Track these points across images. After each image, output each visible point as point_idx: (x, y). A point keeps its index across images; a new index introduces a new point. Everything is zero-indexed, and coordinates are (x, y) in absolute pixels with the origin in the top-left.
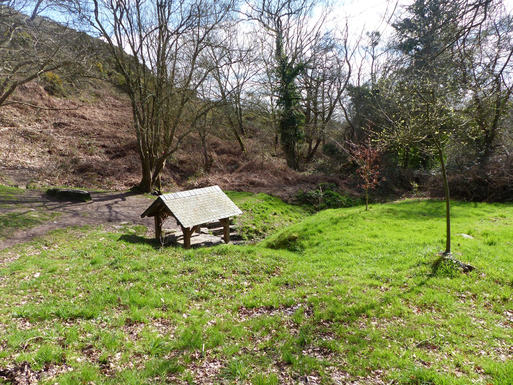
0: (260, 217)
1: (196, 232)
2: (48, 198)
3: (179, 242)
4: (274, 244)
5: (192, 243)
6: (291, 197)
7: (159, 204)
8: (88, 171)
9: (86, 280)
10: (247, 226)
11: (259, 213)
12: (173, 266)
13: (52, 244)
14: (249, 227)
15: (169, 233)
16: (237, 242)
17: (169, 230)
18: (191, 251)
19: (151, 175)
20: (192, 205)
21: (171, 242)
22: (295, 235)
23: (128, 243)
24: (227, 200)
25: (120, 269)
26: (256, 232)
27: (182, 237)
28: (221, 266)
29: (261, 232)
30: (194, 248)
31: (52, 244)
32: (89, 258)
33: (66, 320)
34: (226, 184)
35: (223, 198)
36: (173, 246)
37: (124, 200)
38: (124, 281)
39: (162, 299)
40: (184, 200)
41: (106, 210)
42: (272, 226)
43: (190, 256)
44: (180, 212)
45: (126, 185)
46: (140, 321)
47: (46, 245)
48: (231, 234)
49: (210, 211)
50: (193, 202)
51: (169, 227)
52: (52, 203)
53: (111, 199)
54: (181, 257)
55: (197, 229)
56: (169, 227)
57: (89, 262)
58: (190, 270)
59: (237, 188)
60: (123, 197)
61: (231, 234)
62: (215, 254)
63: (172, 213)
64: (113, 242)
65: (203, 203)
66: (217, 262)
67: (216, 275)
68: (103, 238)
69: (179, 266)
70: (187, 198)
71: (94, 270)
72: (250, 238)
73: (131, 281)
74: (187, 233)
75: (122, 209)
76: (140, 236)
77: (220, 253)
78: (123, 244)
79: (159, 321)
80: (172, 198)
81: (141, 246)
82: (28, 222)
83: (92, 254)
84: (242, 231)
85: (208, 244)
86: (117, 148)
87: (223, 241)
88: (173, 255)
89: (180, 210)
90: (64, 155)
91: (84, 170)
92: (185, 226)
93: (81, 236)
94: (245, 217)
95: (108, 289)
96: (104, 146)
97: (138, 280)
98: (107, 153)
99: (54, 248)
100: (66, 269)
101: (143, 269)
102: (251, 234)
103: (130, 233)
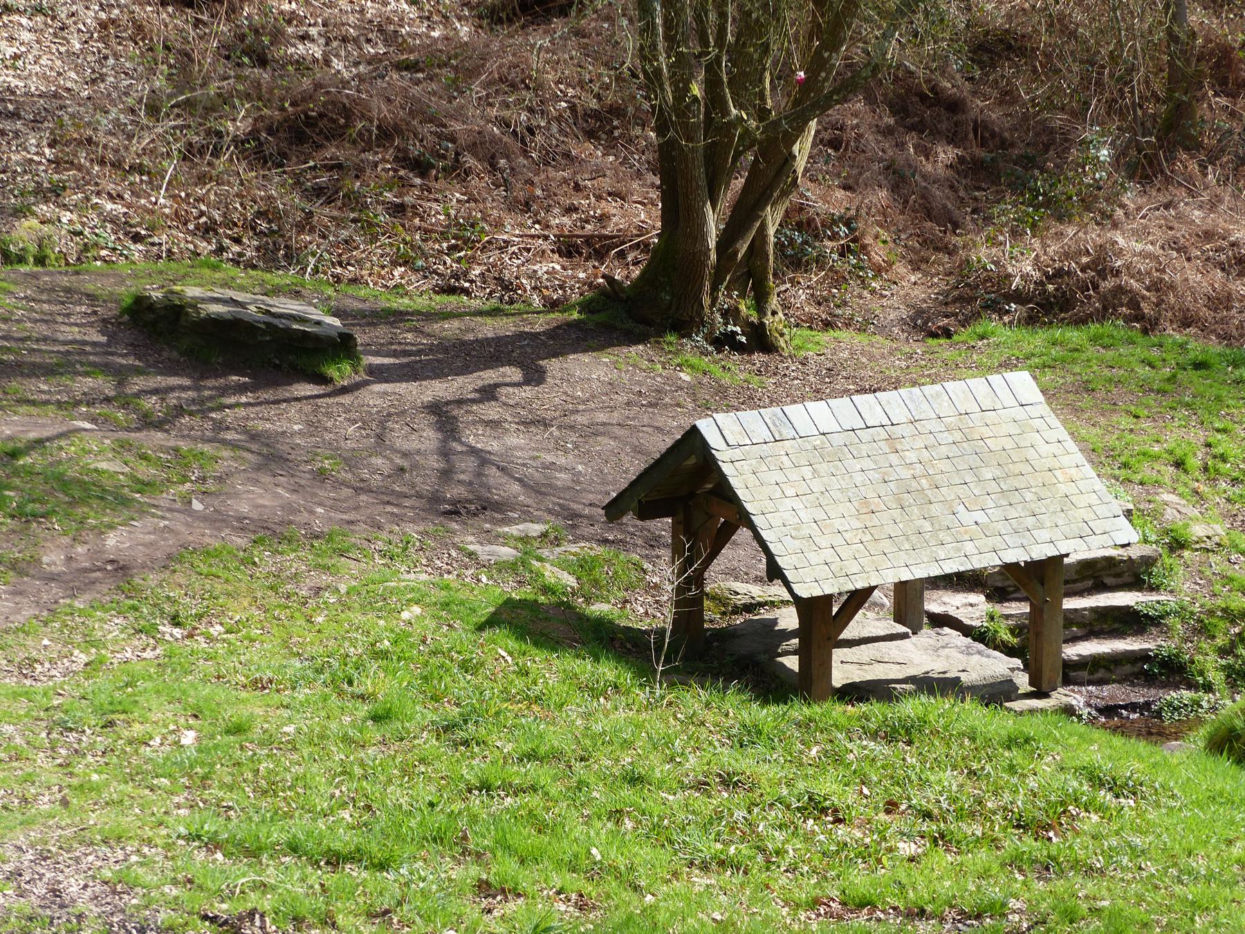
2: (135, 349)
5: (839, 677)
7: (692, 461)
8: (337, 134)
9: (358, 771)
13: (199, 617)
15: (750, 608)
18: (840, 711)
19: (713, 224)
20: (859, 478)
23: (528, 647)
24: (1065, 460)
25: (476, 749)
31: (199, 617)
32: (362, 697)
33: (317, 862)
35: (1044, 449)
37: (535, 376)
38: (485, 787)
39: (594, 851)
40: (825, 451)
41: (428, 438)
45: (568, 249)
46: (515, 889)
47: (175, 621)
49: (948, 520)
50: (867, 464)
51: (732, 578)
53: (465, 370)
57: (364, 709)
58: (728, 781)
60: (529, 355)
64: (460, 636)
65: (919, 469)
67: (816, 807)
68: (417, 610)
70: (838, 440)
71: (384, 743)
73: (518, 791)
74: (824, 620)
75: (514, 440)
76: (599, 609)
77: (889, 734)
78: (503, 648)
79: (569, 900)
81: (584, 667)
82: (81, 494)
83: (376, 681)
84: (1202, 630)
91: (304, 131)
93: (318, 591)
95: (432, 805)
99: (210, 639)
100: (286, 729)
101: (556, 756)
103: (546, 590)
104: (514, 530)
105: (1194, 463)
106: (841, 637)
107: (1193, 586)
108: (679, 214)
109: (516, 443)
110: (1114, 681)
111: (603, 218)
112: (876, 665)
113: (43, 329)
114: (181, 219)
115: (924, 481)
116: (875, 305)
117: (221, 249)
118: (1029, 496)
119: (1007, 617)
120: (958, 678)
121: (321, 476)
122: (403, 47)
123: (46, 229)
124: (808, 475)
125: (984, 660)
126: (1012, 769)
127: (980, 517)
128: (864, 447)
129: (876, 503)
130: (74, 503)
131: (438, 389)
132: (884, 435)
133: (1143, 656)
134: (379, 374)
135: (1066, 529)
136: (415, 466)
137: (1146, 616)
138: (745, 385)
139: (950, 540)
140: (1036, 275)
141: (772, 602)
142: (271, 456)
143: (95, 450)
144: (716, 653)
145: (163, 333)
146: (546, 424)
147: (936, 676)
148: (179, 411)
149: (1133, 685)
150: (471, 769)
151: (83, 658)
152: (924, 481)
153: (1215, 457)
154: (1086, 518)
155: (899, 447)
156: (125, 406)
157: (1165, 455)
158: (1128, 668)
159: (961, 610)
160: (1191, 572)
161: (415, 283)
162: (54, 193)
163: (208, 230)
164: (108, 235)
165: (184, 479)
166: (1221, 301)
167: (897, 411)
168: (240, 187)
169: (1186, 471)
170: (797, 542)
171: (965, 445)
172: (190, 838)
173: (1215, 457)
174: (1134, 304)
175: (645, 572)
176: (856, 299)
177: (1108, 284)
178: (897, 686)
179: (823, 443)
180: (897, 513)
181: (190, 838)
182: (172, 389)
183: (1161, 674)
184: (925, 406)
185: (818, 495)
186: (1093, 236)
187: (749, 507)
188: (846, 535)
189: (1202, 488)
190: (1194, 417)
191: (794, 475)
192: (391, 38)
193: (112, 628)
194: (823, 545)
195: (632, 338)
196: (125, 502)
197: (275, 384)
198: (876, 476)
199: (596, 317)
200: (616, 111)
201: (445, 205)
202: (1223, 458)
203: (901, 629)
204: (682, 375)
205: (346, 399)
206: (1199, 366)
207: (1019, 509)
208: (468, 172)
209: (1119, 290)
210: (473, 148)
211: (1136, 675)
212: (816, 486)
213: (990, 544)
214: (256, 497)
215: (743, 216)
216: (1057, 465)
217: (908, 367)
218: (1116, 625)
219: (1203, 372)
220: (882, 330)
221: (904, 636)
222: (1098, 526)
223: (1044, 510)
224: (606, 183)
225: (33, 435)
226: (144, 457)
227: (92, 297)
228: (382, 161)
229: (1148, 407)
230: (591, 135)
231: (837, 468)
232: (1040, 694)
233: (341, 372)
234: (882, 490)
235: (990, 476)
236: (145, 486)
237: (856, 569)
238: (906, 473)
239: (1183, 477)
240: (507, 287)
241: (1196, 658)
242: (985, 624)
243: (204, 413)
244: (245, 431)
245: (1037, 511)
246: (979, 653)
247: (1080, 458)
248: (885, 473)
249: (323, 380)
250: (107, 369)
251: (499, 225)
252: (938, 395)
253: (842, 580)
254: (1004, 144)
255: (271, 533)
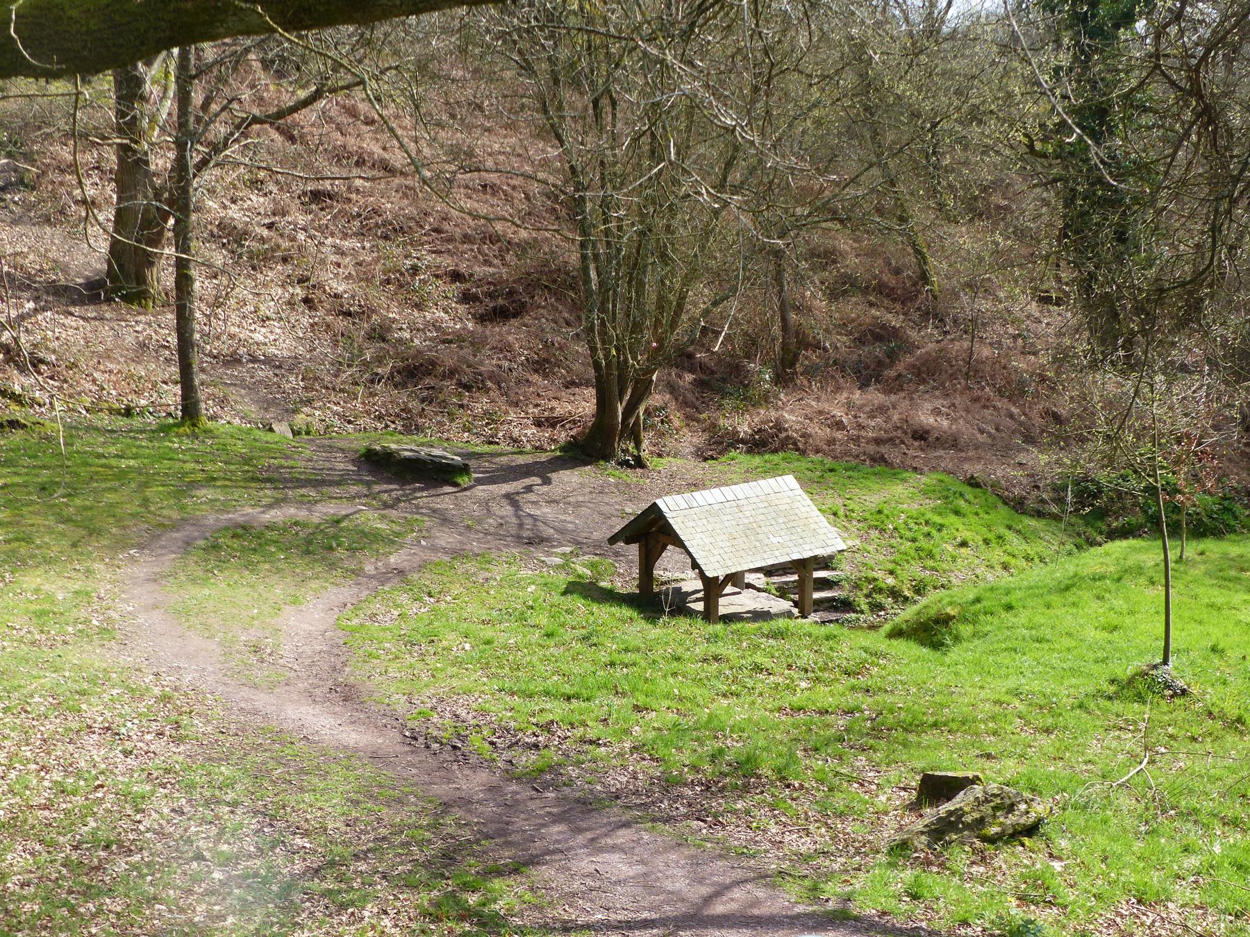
0: (913, 553)
2: (370, 473)
3: (692, 605)
4: (904, 627)
5: (722, 611)
6: (1037, 487)
10: (871, 574)
11: (914, 540)
14: (875, 580)
16: (833, 616)
17: (669, 574)
18: (719, 627)
20: (727, 524)
21: (678, 605)
22: (950, 611)
24: (812, 514)
26: (894, 593)
27: (700, 595)
29: (906, 593)
30: (725, 623)
34: (839, 435)
35: (803, 509)
37: (547, 481)
38: (612, 664)
40: (711, 512)
41: (508, 510)
42: (944, 581)
43: (717, 636)
45: (538, 424)
50: (729, 517)
51: (671, 570)
52: (385, 487)
53: (515, 479)
55: (735, 579)
56: (671, 570)
58: (716, 658)
59: (871, 449)
60: (542, 471)
62: (763, 635)
63: (682, 541)
64: (557, 599)
65: (751, 520)
67: (758, 668)
68: (533, 587)
70: (716, 507)
72: (877, 607)
74: (713, 588)
77: (778, 635)
78: (578, 603)
80: (683, 505)
82: (368, 539)
84: (857, 587)
85: (760, 616)
86: (496, 282)
87: (796, 611)
88: (686, 632)
89: (699, 535)
90: (349, 314)
91: (413, 371)
92: (710, 574)
94: (870, 548)
96: (456, 276)
97: (634, 664)
98: (466, 298)
102: (879, 598)
103: (579, 576)
104: (559, 550)
105: (841, 513)
108: (604, 405)
109: (546, 511)
111: (552, 409)
113: (327, 465)
114: (368, 413)
116: (679, 446)
117: (387, 426)
121: (468, 527)
122: (445, 333)
123: (309, 419)
126: (831, 649)
127: (779, 539)
130: (371, 542)
131: (506, 488)
133: (833, 599)
134: (479, 482)
136: (507, 522)
140: (750, 431)
142: (445, 520)
143: (370, 518)
144: (651, 601)
145: (379, 464)
146: (557, 502)
148: (398, 500)
150: (603, 657)
151: (396, 613)
156: (374, 499)
161: (474, 440)
162: (309, 402)
163: (380, 418)
164: (337, 422)
165: (412, 531)
166: (831, 442)
168: (385, 396)
172: (500, 691)
174: (795, 444)
176: (670, 443)
177: (783, 435)
181: (500, 691)
182: (392, 490)
186: (773, 414)
191: (700, 523)
192: (438, 329)
193: (404, 599)
195: (585, 464)
196: (393, 542)
197: (435, 487)
199: (569, 454)
200: (546, 360)
201: (481, 404)
203: (737, 590)
205: (467, 493)
206: (831, 470)
208: (489, 389)
209: (788, 437)
210: (490, 378)
214: (446, 538)
215: (631, 409)
220: (683, 457)
224: (550, 394)
225: (344, 513)
226: (393, 522)
227: (342, 450)
228: (450, 385)
230: (536, 371)
232: (804, 617)
233: (464, 481)
236: (397, 534)
238: (746, 521)
240: (515, 441)
243: (409, 501)
244: (429, 508)
249: (456, 485)
250: (361, 482)
251: (506, 413)
254: (713, 373)
255: (457, 554)
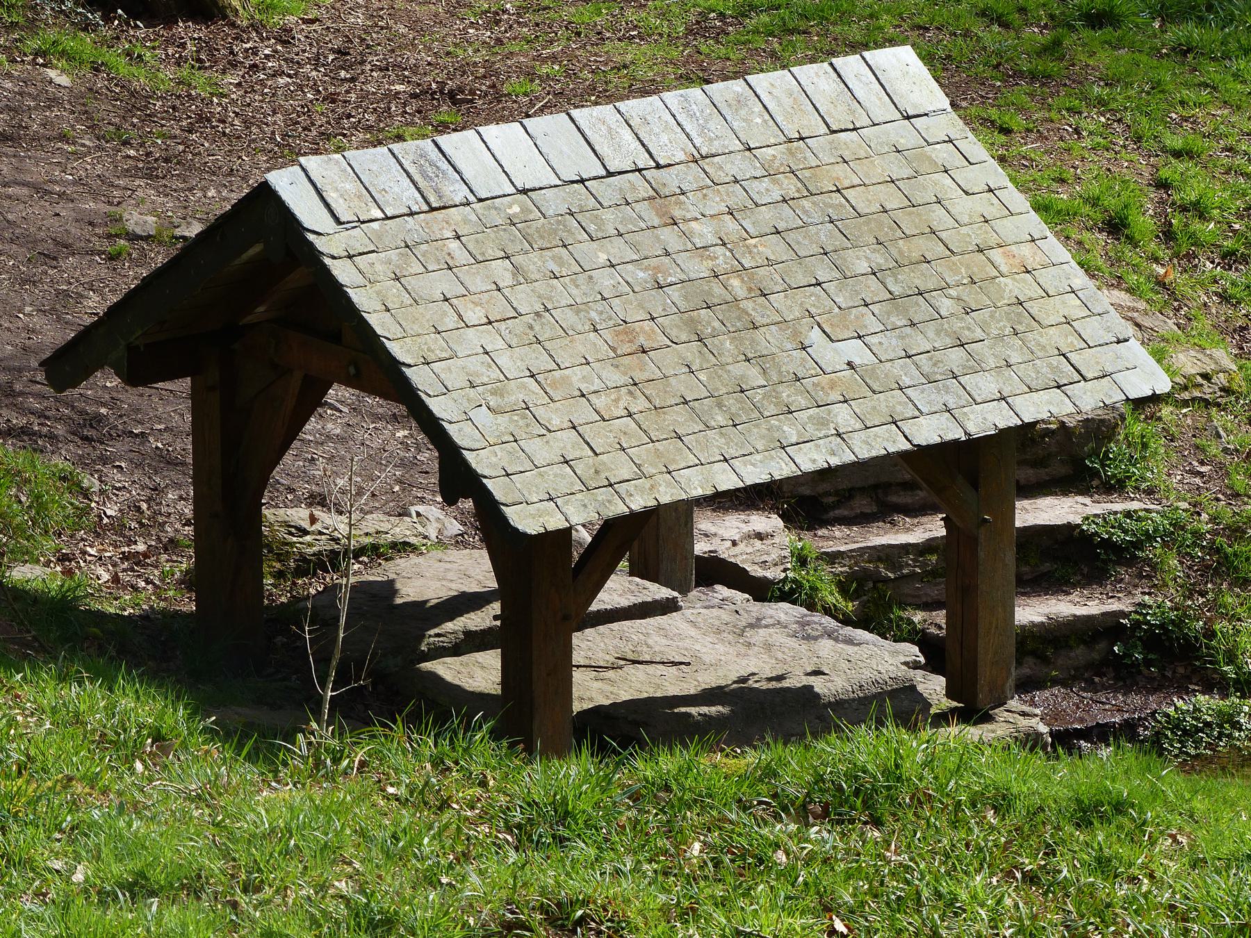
1: (642, 570)
3: (447, 669)
5: (589, 692)
12: (431, 880)
15: (333, 560)
16: (1109, 708)
17: (336, 523)
18: (574, 773)
20: (606, 280)
27: (483, 619)
28: (811, 901)
30: (601, 750)
35: (963, 207)
36: (414, 720)
40: (528, 226)
43: (564, 815)
44: (476, 365)
48: (1031, 612)
49: (793, 361)
50: (618, 250)
51: (338, 495)
54: (485, 817)
55: (651, 540)
56: (338, 495)
61: (1031, 612)
62: (781, 806)
66: (788, 874)
69: (474, 878)
70: (554, 202)
74: (544, 583)
81: (87, 697)
87: (933, 687)
88: (419, 798)
92: (528, 519)
101: (194, 886)
105: (1144, 222)
106: (594, 607)
107: (1189, 479)
110: (1055, 682)
112: (630, 669)
115: (735, 282)
118: (946, 306)
119: (832, 558)
120: (809, 688)
124: (506, 280)
125: (850, 649)
126: (1103, 865)
127: (854, 351)
128: (607, 215)
129: (648, 334)
132: (644, 191)
133: (1108, 627)
135: (1028, 372)
137: (1108, 544)
138: (182, 90)
139: (804, 403)
141: (375, 548)
144: (265, 653)
147: (764, 685)
149: (1092, 687)
152: (735, 282)
153: (1184, 209)
154: (1075, 346)
155: (677, 213)
157: (1087, 209)
158: (1080, 654)
159: (741, 547)
160: (1179, 451)
167: (664, 138)
169: (1133, 242)
170: (501, 419)
171: (804, 202)
173: (1184, 209)
175: (86, 494)
178: (693, 710)
179: (524, 210)
180: (691, 351)
183: (1148, 663)
184: (716, 125)
185: (529, 319)
187: (397, 350)
188: (599, 402)
189: (1174, 276)
190: (1119, 128)
194: (556, 422)
198: (641, 275)
202: (1198, 210)
204: (52, 73)
207: (931, 334)
211: (1098, 668)
212: (525, 299)
213: (883, 408)
216: (993, 240)
217: (499, 41)
218: (1047, 567)
219: (1107, 33)
221: (668, 607)
222: (1088, 361)
223: (979, 334)
229: (1021, 109)
231: (559, 260)
232: (972, 711)
234: (656, 301)
235: (863, 267)
237: (626, 471)
238: (697, 268)
239: (1128, 253)
241: (1217, 627)
242: (791, 575)
245: (966, 336)
246: (830, 635)
247: (1034, 223)
248: (657, 269)
252: (740, 102)
253: (603, 494)
